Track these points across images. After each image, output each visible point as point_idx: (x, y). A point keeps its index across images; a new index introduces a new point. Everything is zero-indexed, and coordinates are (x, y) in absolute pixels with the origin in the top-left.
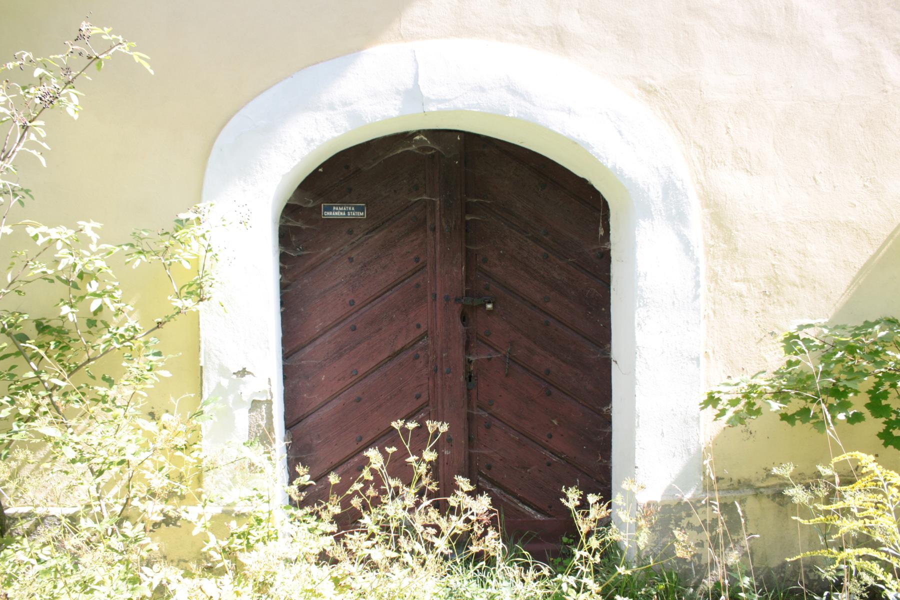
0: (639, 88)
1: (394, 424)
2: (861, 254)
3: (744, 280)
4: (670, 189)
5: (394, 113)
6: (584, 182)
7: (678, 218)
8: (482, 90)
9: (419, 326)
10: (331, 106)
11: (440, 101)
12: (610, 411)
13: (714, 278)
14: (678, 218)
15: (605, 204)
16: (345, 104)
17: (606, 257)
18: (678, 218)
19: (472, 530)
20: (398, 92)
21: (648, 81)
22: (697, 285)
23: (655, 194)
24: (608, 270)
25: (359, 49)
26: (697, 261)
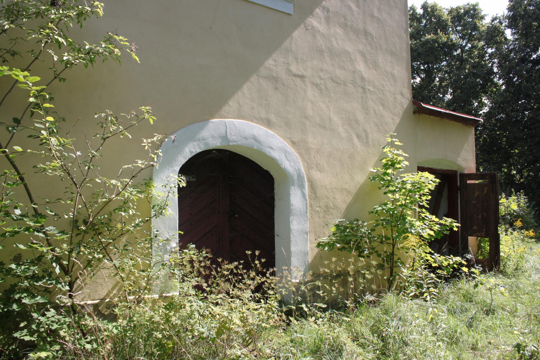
0: (291, 141)
1: (247, 252)
2: (349, 199)
3: (319, 207)
4: (300, 176)
5: (219, 144)
6: (267, 171)
7: (301, 187)
8: (246, 138)
9: (213, 223)
10: (199, 140)
11: (234, 141)
12: (274, 254)
13: (311, 206)
14: (302, 187)
15: (273, 179)
16: (204, 140)
17: (273, 199)
18: (301, 187)
19: (145, 341)
20: (221, 137)
21: (293, 139)
22: (307, 208)
23: (295, 178)
24: (274, 203)
25: (208, 120)
26: (307, 200)
